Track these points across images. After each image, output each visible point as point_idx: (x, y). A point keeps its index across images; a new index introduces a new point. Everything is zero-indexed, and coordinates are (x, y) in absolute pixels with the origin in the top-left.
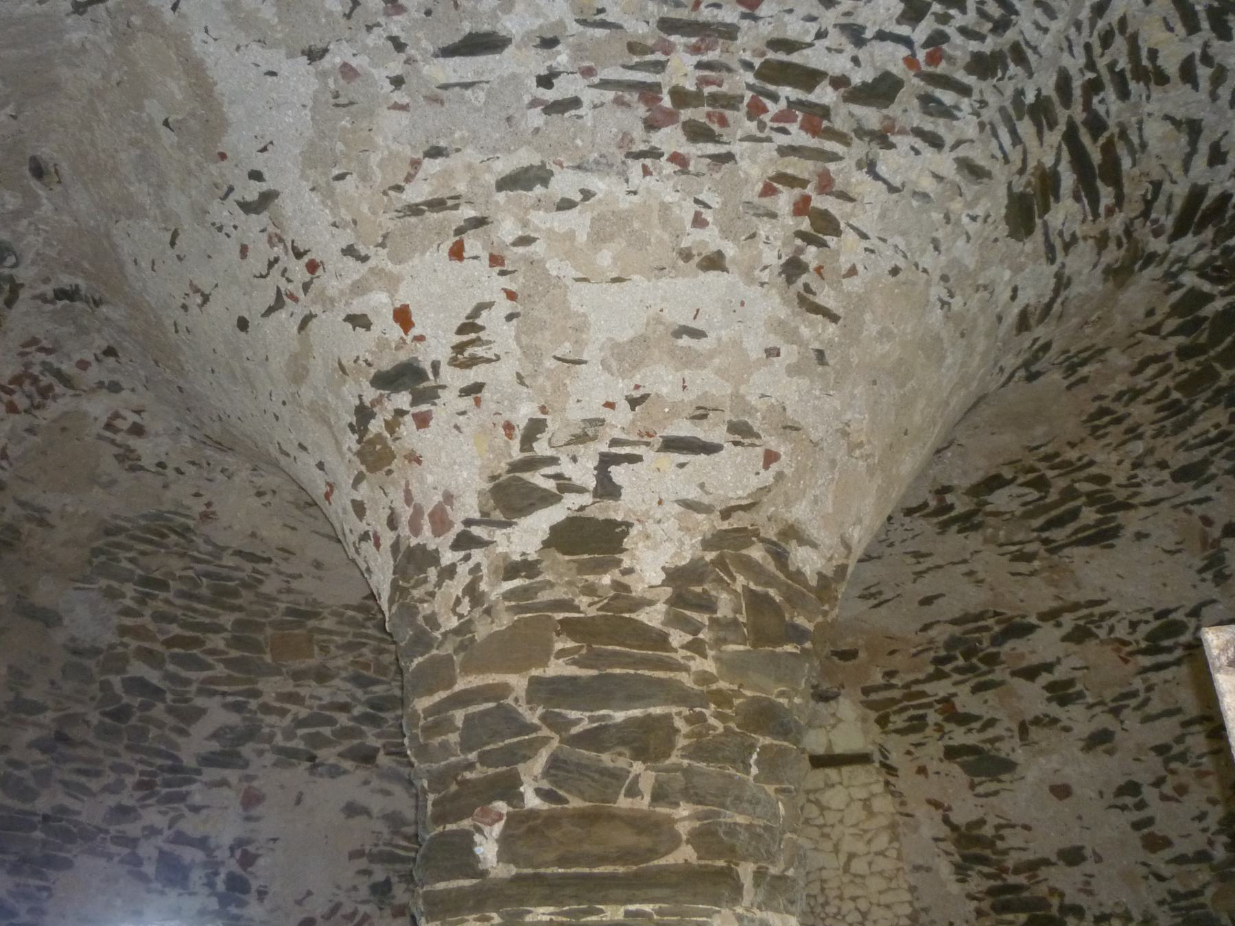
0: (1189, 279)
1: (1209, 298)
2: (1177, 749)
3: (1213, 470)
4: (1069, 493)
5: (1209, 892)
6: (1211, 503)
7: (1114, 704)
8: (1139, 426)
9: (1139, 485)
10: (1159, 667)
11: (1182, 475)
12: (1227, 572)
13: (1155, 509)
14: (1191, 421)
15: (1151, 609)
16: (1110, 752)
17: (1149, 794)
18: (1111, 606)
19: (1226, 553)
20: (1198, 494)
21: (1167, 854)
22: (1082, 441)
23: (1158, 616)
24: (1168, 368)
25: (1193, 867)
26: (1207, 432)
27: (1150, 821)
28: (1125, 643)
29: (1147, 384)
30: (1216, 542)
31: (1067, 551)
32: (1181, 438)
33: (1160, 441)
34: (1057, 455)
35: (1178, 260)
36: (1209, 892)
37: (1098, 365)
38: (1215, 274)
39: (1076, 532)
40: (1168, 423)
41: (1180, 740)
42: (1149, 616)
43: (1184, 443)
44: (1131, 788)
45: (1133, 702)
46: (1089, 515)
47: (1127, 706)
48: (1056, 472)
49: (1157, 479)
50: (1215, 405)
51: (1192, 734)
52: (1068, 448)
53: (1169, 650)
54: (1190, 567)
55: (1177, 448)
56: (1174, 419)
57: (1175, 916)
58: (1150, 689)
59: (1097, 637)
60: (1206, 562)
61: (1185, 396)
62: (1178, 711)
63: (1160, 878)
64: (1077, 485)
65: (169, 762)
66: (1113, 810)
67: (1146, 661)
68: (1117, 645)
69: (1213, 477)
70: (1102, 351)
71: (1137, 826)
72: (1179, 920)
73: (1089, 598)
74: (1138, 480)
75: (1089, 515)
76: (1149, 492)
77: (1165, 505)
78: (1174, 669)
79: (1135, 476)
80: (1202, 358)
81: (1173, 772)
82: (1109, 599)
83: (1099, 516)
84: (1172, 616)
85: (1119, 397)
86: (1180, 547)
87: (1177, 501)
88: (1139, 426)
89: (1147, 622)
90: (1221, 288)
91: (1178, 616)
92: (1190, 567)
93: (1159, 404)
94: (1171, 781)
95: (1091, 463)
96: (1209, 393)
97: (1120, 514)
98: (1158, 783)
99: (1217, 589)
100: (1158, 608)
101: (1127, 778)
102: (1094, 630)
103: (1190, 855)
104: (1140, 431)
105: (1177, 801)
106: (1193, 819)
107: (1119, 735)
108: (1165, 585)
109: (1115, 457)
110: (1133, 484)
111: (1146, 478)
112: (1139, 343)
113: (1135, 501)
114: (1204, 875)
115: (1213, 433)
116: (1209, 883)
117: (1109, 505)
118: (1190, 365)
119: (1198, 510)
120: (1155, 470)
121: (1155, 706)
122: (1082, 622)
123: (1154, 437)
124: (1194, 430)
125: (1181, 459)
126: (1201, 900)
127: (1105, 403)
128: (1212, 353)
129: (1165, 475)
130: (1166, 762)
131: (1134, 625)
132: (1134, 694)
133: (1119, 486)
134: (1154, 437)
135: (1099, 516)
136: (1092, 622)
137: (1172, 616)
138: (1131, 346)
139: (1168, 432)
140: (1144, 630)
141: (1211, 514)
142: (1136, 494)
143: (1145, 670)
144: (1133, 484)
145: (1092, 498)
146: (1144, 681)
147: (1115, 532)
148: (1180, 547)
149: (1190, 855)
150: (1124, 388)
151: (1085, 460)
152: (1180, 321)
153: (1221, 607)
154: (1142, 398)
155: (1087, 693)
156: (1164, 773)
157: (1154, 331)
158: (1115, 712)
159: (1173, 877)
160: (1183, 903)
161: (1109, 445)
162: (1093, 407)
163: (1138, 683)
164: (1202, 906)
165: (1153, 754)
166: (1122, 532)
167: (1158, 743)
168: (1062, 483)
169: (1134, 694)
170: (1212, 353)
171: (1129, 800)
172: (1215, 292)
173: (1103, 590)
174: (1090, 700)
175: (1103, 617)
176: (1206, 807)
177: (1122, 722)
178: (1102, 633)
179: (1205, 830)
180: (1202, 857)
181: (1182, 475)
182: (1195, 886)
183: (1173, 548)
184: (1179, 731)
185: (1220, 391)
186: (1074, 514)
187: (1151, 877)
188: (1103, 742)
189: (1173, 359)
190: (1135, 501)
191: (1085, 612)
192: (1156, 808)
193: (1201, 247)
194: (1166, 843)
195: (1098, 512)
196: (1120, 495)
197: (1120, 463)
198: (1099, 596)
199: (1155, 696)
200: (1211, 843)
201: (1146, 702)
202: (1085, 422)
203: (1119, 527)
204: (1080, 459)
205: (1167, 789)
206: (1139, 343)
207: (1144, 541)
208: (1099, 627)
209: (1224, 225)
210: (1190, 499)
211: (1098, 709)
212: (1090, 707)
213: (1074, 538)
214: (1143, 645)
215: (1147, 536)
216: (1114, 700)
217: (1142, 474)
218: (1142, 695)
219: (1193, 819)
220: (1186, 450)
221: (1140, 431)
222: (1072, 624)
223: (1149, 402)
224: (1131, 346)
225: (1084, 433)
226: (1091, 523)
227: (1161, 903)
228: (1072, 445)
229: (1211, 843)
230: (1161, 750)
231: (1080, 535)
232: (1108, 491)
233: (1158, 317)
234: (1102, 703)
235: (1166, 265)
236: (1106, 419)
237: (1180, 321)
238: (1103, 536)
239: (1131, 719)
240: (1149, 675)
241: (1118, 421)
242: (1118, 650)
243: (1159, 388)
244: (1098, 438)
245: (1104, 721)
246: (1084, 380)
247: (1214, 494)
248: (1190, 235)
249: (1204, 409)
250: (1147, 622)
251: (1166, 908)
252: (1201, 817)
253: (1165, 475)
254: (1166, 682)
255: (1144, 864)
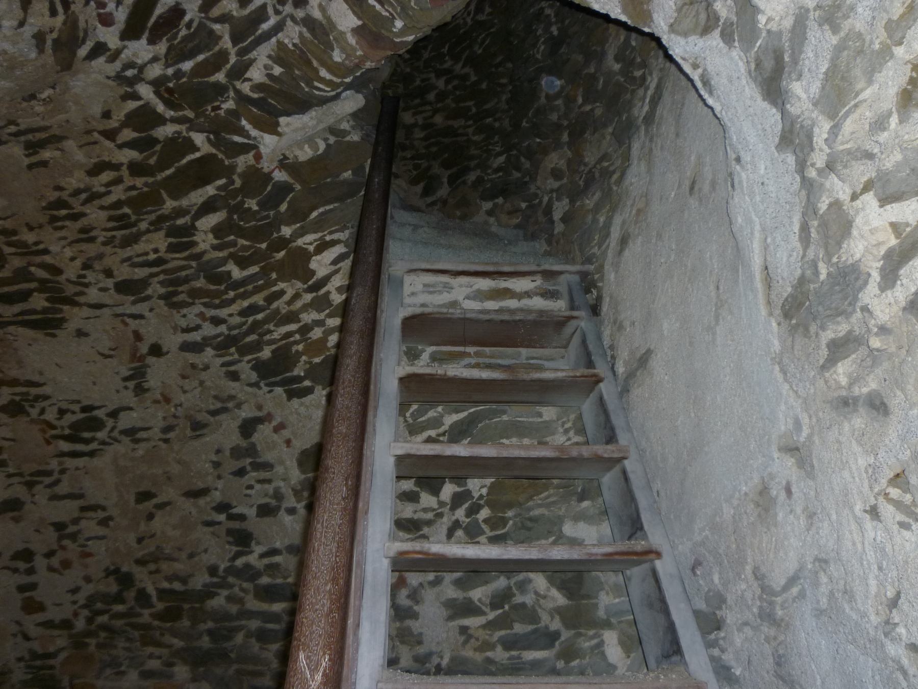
0: (145, 91)
1: (161, 120)
2: (71, 529)
3: (149, 291)
4: (22, 275)
5: (63, 656)
6: (143, 322)
7: (29, 478)
8: (93, 229)
9: (86, 285)
10: (75, 455)
11: (124, 287)
12: (146, 385)
13: (98, 312)
14: (134, 239)
15: (79, 402)
16: (16, 520)
17: (40, 562)
18: (47, 390)
19: (149, 370)
20: (135, 310)
21: (40, 617)
22: (41, 226)
23: (84, 409)
24: (118, 181)
25: (56, 632)
26: (147, 254)
27: (33, 586)
28: (53, 427)
29: (103, 189)
30: (142, 358)
31: (11, 329)
32: (128, 252)
33: (108, 249)
34: (14, 233)
35: (130, 65)
36: (63, 656)
37: (57, 153)
38: (166, 95)
39: (22, 313)
40: (119, 234)
41: (76, 521)
42: (76, 407)
43: (129, 259)
44: (26, 555)
45: (48, 480)
46: (39, 302)
47: (41, 482)
48: (13, 250)
49: (101, 285)
50: (156, 230)
51: (87, 519)
52: (25, 230)
53: (87, 441)
54: (117, 373)
55: (124, 261)
56: (123, 232)
57: (26, 673)
58: (63, 471)
59: (28, 415)
60: (132, 372)
61: (134, 213)
62: (81, 496)
63: (27, 638)
64: (33, 269)
65: (175, 299)
66: (6, 571)
67: (65, 446)
68: (44, 426)
69: (148, 298)
70: (59, 139)
71: (22, 589)
72: (30, 676)
73: (28, 378)
74: (86, 281)
75: (39, 302)
76: (93, 295)
77: (106, 311)
78: (86, 458)
79: (84, 276)
80: (150, 180)
81: (63, 548)
82: (44, 384)
83: (47, 304)
84: (96, 413)
85: (77, 193)
86: (112, 353)
87: (119, 310)
88: (93, 229)
89: (74, 413)
90: (172, 113)
91: (100, 413)
92: (117, 373)
93: (113, 213)
94: (60, 555)
95: (46, 252)
96: (153, 217)
97: (66, 308)
98: (50, 554)
99: (135, 399)
100: (86, 402)
101: (24, 546)
102: (28, 408)
103: (57, 622)
104: (92, 234)
105: (61, 574)
106: (68, 592)
107: (27, 507)
108: (94, 383)
109: (68, 252)
110: (81, 282)
111: (93, 281)
112: (95, 143)
113: (82, 299)
114: (61, 642)
115: (152, 257)
116: (63, 649)
117: (60, 298)
118: (139, 182)
119: (133, 324)
120: (101, 276)
121: (63, 488)
122: (17, 398)
123: (104, 244)
124: (140, 247)
125: (124, 272)
126: (51, 662)
127: (64, 195)
128: (160, 177)
129: (110, 283)
130: (60, 538)
131: (62, 412)
132: (48, 473)
133: (68, 280)
134: (104, 244)
135: (47, 304)
136: (27, 400)
137: (96, 413)
138: (89, 144)
139: (117, 242)
140: (69, 419)
141: (142, 331)
142: (82, 294)
143: (63, 454)
144: (81, 282)
145: (44, 285)
146: (60, 464)
147: (58, 324)
148: (112, 353)
149: (57, 622)
150: (82, 186)
151: (41, 247)
152: (135, 135)
153: (135, 415)
154: (96, 202)
155: (10, 463)
156: (55, 547)
157: (110, 135)
158: (30, 485)
159: (36, 639)
160: (38, 663)
161: (65, 238)
162: (53, 196)
163: (54, 464)
164: (52, 667)
165: (51, 528)
166: (65, 325)
167: (57, 520)
168: (17, 263)
169: (48, 473)
170: (160, 177)
171: (22, 565)
172: (167, 116)
173: (41, 373)
174: (11, 470)
175: (37, 398)
176: (81, 583)
177: (33, 495)
178: (34, 412)
179: (74, 603)
180: (66, 624)
181: (124, 287)
182: (52, 649)
183: (106, 352)
184: (76, 514)
185: (161, 219)
186: (25, 296)
187: (19, 636)
188: (13, 510)
189: (125, 172)
190: (82, 299)
191: (24, 389)
192: (42, 576)
193: (155, 59)
194: (41, 608)
195: (47, 300)
196: (70, 290)
197: (73, 259)
198: (36, 378)
199: (65, 478)
200: (76, 614)
201: (57, 482)
202: (44, 208)
203: (63, 320)
204: (36, 244)
205: (55, 561)
206: (95, 143)
207: (83, 339)
208: (32, 406)
209: (176, 42)
210: (128, 312)
211: (16, 480)
212: (10, 476)
213: (20, 318)
214: (67, 432)
215: (86, 335)
216: (31, 475)
217: (91, 277)
218: (56, 476)
219: (68, 592)
220: (131, 266)
221: (92, 234)
222: (9, 398)
223: (102, 208)
224: (89, 144)
225: (43, 219)
226: (39, 308)
227: (20, 659)
228: (31, 229)
229: (76, 614)
230: (59, 527)
231: (27, 317)
232: (58, 282)
233: (113, 124)
234: (20, 475)
235: (118, 65)
236: (64, 212)
237: (135, 135)
238: (48, 324)
239: (41, 494)
240: (66, 459)
241: (75, 217)
242: (43, 431)
243: (112, 198)
244: (56, 229)
245: (19, 491)
246: (44, 164)
247: (147, 314)
248: (144, 41)
249: (148, 231)
250: (74, 413)
251: (22, 664)
252: (75, 591)
253: (110, 283)
254: (77, 469)
255: (18, 623)
